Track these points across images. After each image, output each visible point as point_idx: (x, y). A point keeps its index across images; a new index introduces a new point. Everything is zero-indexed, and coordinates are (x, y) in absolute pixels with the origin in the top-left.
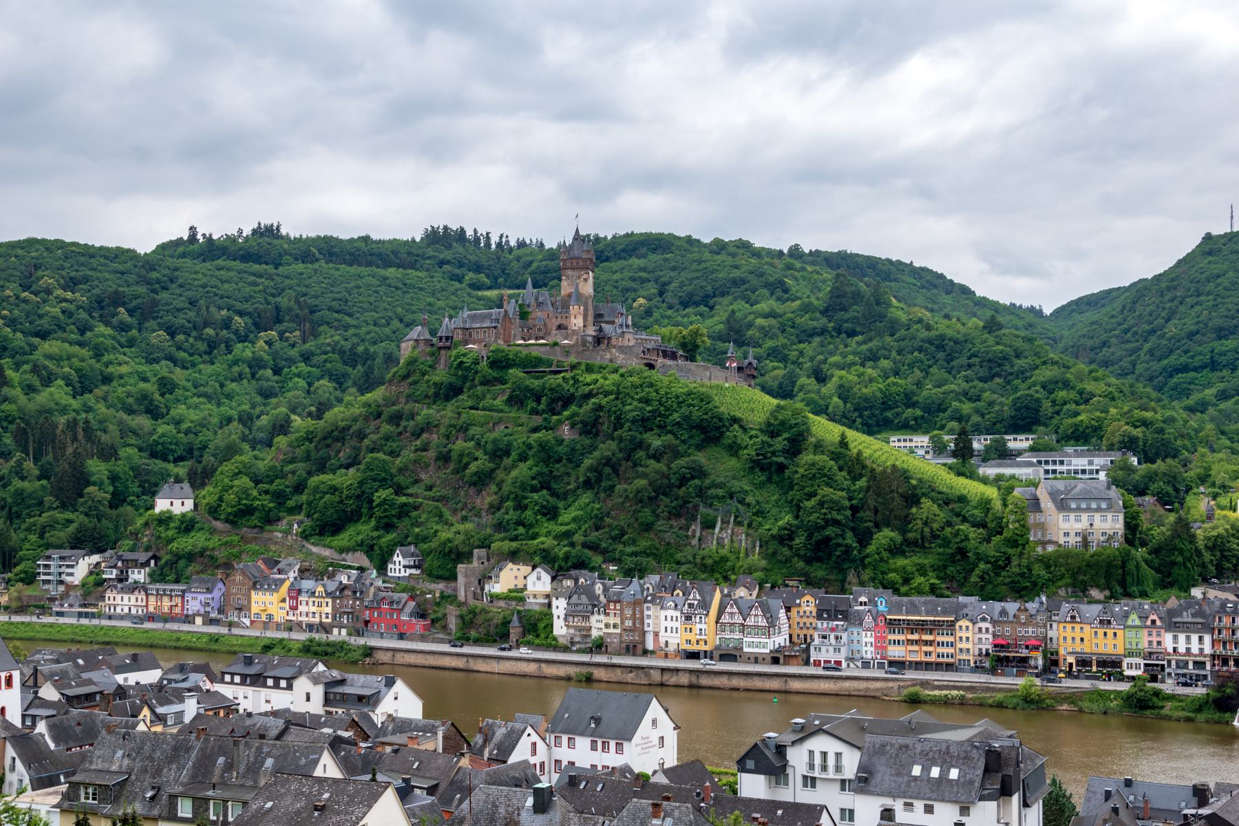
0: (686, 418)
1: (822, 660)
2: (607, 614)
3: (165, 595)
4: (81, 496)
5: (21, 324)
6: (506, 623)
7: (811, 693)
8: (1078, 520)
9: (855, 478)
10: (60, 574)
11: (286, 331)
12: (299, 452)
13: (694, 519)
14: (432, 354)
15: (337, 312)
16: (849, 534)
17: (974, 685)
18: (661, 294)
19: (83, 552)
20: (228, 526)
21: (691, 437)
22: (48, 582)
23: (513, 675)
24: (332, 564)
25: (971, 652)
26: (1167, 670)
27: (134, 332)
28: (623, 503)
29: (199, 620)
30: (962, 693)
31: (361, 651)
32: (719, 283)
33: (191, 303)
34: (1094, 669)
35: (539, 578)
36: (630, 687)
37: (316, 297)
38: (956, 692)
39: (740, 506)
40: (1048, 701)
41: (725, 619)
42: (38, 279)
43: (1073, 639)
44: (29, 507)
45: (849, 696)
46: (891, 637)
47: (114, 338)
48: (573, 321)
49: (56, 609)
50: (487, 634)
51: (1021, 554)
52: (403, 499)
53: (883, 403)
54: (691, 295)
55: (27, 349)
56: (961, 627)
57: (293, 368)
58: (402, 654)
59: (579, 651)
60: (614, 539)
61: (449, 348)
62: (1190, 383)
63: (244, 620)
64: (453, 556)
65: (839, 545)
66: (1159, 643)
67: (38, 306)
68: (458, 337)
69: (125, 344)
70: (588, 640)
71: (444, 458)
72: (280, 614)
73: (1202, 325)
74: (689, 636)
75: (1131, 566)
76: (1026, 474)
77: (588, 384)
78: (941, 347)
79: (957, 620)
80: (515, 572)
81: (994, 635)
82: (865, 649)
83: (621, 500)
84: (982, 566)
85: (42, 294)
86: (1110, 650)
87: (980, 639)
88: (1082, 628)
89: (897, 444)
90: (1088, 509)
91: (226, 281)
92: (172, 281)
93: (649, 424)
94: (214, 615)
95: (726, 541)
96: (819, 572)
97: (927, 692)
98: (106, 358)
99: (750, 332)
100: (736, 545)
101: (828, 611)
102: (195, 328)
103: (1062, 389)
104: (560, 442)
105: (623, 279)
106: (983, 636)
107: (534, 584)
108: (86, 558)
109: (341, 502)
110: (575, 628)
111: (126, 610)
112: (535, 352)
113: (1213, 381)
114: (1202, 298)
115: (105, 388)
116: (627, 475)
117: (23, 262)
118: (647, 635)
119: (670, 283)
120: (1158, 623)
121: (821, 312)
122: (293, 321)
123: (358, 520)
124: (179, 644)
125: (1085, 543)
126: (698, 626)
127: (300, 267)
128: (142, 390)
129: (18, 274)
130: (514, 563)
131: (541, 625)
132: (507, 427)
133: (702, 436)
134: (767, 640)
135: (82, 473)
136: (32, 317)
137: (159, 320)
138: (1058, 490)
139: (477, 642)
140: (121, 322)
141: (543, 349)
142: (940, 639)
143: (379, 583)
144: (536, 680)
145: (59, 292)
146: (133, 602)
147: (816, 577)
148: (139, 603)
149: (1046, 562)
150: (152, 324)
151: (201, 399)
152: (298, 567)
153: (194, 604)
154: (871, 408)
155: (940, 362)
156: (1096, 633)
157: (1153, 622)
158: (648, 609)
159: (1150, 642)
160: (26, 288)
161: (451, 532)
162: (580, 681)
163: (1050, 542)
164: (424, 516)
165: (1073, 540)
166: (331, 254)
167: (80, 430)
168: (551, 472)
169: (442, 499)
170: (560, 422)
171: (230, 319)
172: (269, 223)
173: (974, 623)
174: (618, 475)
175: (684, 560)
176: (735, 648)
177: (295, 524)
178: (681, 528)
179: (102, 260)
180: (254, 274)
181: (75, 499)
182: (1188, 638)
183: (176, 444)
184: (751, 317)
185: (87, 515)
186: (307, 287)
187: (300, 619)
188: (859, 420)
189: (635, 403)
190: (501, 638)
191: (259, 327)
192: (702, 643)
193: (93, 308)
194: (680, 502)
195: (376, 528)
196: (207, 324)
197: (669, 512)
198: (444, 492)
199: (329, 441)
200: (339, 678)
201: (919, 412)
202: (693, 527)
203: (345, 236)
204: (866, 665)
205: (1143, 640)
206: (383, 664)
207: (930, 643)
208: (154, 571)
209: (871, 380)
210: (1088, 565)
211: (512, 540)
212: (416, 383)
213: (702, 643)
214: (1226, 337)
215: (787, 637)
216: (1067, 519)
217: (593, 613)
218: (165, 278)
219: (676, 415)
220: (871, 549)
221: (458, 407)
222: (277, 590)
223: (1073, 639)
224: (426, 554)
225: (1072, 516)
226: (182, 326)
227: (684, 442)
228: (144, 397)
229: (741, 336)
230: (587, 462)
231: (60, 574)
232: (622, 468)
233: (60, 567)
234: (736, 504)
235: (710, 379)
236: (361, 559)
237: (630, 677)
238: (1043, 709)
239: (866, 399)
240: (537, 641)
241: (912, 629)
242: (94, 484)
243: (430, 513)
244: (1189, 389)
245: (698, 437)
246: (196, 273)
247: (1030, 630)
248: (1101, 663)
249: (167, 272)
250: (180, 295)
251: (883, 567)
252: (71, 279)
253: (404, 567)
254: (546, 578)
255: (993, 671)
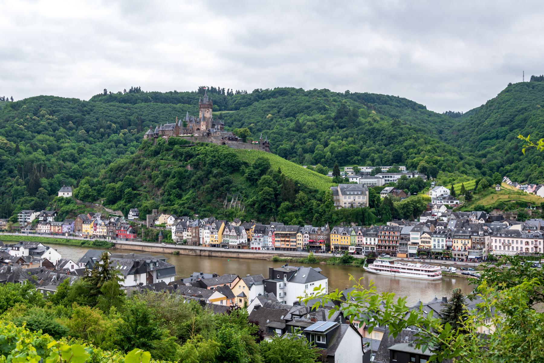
0: (227, 163)
2: (188, 232)
3: (56, 225)
4: (38, 191)
5: (31, 128)
6: (158, 235)
8: (349, 198)
10: (25, 219)
11: (131, 129)
12: (108, 175)
14: (153, 140)
15: (152, 122)
18: (279, 112)
19: (34, 211)
21: (228, 169)
22: (21, 221)
23: (156, 252)
24: (110, 215)
26: (363, 250)
27: (74, 131)
29: (67, 234)
30: (291, 258)
32: (300, 108)
34: (340, 250)
35: (171, 219)
37: (145, 116)
41: (225, 233)
42: (40, 111)
44: (19, 195)
45: (258, 259)
46: (276, 239)
47: (66, 133)
48: (202, 127)
49: (22, 231)
50: (152, 239)
51: (329, 211)
52: (135, 192)
53: (346, 154)
54: (289, 113)
55: (31, 137)
59: (179, 244)
60: (198, 206)
62: (487, 144)
65: (268, 207)
66: (361, 241)
67: (39, 121)
68: (160, 133)
71: (150, 177)
72: (91, 232)
73: (496, 121)
74: (212, 239)
75: (366, 214)
77: (198, 151)
78: (372, 132)
80: (164, 217)
85: (41, 117)
86: (346, 244)
87: (305, 240)
89: (347, 170)
90: (354, 194)
91: (112, 111)
94: (71, 233)
100: (237, 208)
101: (257, 231)
103: (412, 149)
104: (186, 171)
106: (306, 239)
108: (35, 213)
109: (115, 193)
110: (178, 236)
111: (44, 231)
112: (185, 139)
113: (496, 143)
114: (500, 110)
115: (58, 152)
117: (36, 105)
119: (283, 108)
122: (134, 125)
123: (121, 199)
124: (57, 242)
125: (352, 206)
126: (215, 236)
127: (143, 104)
131: (168, 235)
136: (36, 126)
139: (149, 241)
140: (70, 127)
141: (188, 138)
142: (291, 240)
143: (125, 221)
145: (47, 116)
146: (46, 228)
149: (337, 213)
150: (80, 127)
151: (93, 156)
153: (65, 229)
154: (342, 156)
155: (372, 138)
157: (360, 234)
158: (201, 229)
159: (359, 241)
160: (35, 114)
161: (147, 204)
163: (341, 206)
164: (142, 198)
165: (348, 205)
166: (156, 99)
167: (42, 168)
168: (182, 182)
170: (187, 164)
171: (111, 125)
172: (136, 87)
173: (303, 234)
177: (103, 200)
178: (221, 202)
179: (66, 104)
180: (124, 108)
182: (370, 239)
184: (305, 121)
185: (39, 198)
186: (143, 112)
188: (336, 161)
189: (210, 157)
191: (122, 128)
196: (101, 127)
199: (117, 171)
201: (359, 158)
203: (163, 91)
204: (268, 249)
205: (356, 240)
209: (343, 146)
214: (504, 126)
215: (246, 240)
216: (345, 198)
220: (280, 209)
222: (90, 224)
224: (140, 211)
225: (347, 197)
228: (72, 155)
230: (193, 178)
231: (25, 219)
232: (204, 181)
233: (25, 216)
236: (119, 213)
237: (190, 253)
240: (166, 241)
244: (486, 147)
245: (230, 169)
246: (101, 107)
247: (321, 236)
248: (342, 248)
249: (90, 107)
250: (93, 116)
251: (284, 215)
254: (173, 219)
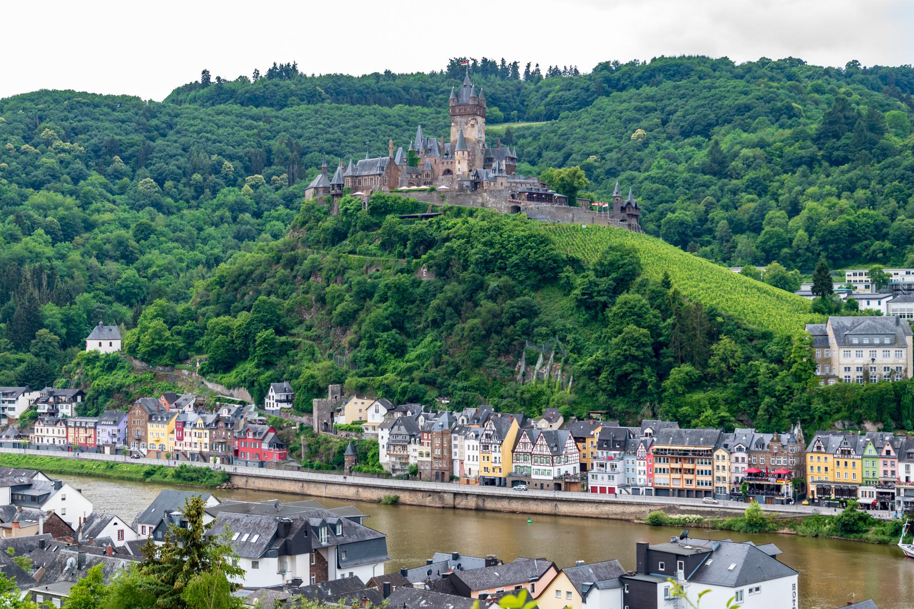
0: (525, 260)
1: (598, 486)
2: (421, 444)
4: (34, 338)
5: (18, 175)
6: (342, 451)
7: (576, 517)
8: (859, 355)
9: (665, 316)
10: (3, 409)
12: (212, 296)
13: (519, 356)
14: (328, 201)
16: (648, 370)
17: (713, 509)
18: (664, 123)
19: (24, 388)
20: (144, 364)
21: (528, 278)
24: (219, 399)
25: (727, 480)
26: (897, 498)
28: (460, 341)
29: (107, 450)
30: (699, 516)
31: (221, 478)
33: (184, 150)
34: (833, 497)
35: (377, 411)
36: (428, 509)
37: (310, 139)
38: (694, 516)
39: (560, 343)
40: (770, 525)
41: (521, 448)
42: (41, 131)
43: (819, 468)
45: (608, 519)
46: (658, 465)
48: (458, 166)
50: (328, 462)
51: (804, 389)
54: (693, 124)
55: (17, 198)
56: (718, 456)
57: (272, 211)
58: (253, 479)
59: (398, 478)
60: (449, 375)
61: (340, 195)
63: (142, 450)
64: (315, 391)
65: (637, 380)
66: (893, 473)
68: (348, 184)
69: (117, 191)
70: (407, 467)
71: (322, 300)
76: (901, 310)
77: (448, 229)
79: (715, 449)
81: (750, 465)
82: (639, 477)
83: (458, 338)
84: (767, 399)
86: (850, 479)
87: (737, 468)
88: (826, 458)
90: (871, 345)
92: (171, 127)
93: (491, 266)
94: (118, 446)
95: (546, 377)
96: (620, 406)
97: (671, 516)
98: (94, 206)
99: (733, 163)
100: (553, 380)
101: (607, 442)
102: (185, 174)
104: (417, 284)
105: (627, 110)
106: (740, 465)
107: (373, 416)
108: (27, 394)
109: (232, 342)
110: (396, 456)
111: (51, 442)
112: (413, 198)
115: (86, 235)
116: (467, 315)
117: (30, 114)
118: (455, 462)
119: (676, 111)
120: (893, 453)
121: (813, 140)
122: (281, 164)
123: (246, 359)
124: (82, 471)
125: (866, 376)
126: (494, 455)
127: (303, 108)
128: (118, 236)
129: (23, 126)
130: (358, 397)
131: (370, 454)
132: (378, 270)
133: (539, 277)
134: (551, 468)
135: (37, 317)
136: (29, 168)
137: (152, 167)
138: (844, 326)
139: (319, 469)
140: (116, 170)
141: (421, 195)
142: (699, 467)
143: (256, 416)
144: (355, 503)
145: (58, 143)
146: (56, 434)
147: (617, 410)
148: (61, 435)
149: (825, 397)
151: (176, 244)
152: (193, 401)
153: (104, 434)
156: (838, 462)
157: (888, 452)
158: (455, 439)
159: (885, 472)
160: (27, 139)
162: (386, 504)
163: (834, 377)
164: (300, 354)
169: (317, 338)
171: (220, 164)
172: (285, 63)
174: (460, 315)
175: (505, 394)
176: (526, 476)
177: (199, 361)
178: (509, 365)
179: (106, 110)
180: (252, 118)
181: (29, 341)
183: (139, 288)
185: (37, 355)
186: (303, 128)
187: (185, 449)
188: (823, 254)
189: (480, 246)
190: (338, 465)
191: (249, 171)
192: (497, 470)
193: (90, 157)
194: (508, 340)
195: (258, 366)
196: (195, 170)
197: (499, 350)
198: (319, 332)
199: (236, 285)
200: (26, 483)
201: (887, 244)
202: (520, 363)
204: (636, 491)
205: (879, 470)
206: (238, 488)
207: (691, 471)
208: (80, 406)
209: (842, 212)
210: (862, 399)
211: (361, 376)
212: (310, 229)
213: (497, 470)
216: (847, 354)
217: (410, 443)
218: (164, 125)
219: (515, 257)
220: (667, 383)
221: (339, 252)
223: (819, 468)
224: (296, 388)
225: (853, 351)
226: (172, 173)
227: (521, 282)
229: (724, 168)
230: (434, 303)
233: (3, 402)
234: (558, 341)
235: (573, 221)
236: (243, 394)
237: (428, 501)
238: (766, 532)
239: (831, 232)
241: (677, 459)
242: (47, 327)
243: (305, 351)
245: (535, 277)
247: (782, 459)
248: (840, 491)
249: (167, 118)
250: (175, 142)
252: (73, 129)
253: (277, 401)
254: (383, 410)
255: (745, 499)
